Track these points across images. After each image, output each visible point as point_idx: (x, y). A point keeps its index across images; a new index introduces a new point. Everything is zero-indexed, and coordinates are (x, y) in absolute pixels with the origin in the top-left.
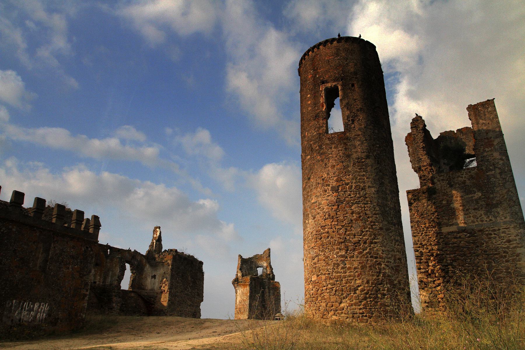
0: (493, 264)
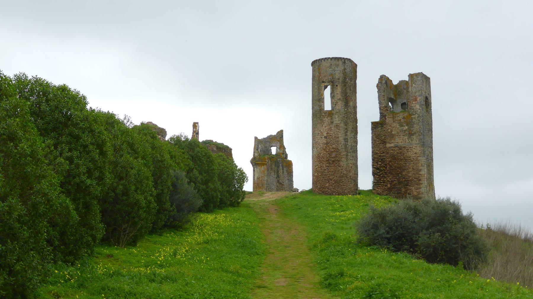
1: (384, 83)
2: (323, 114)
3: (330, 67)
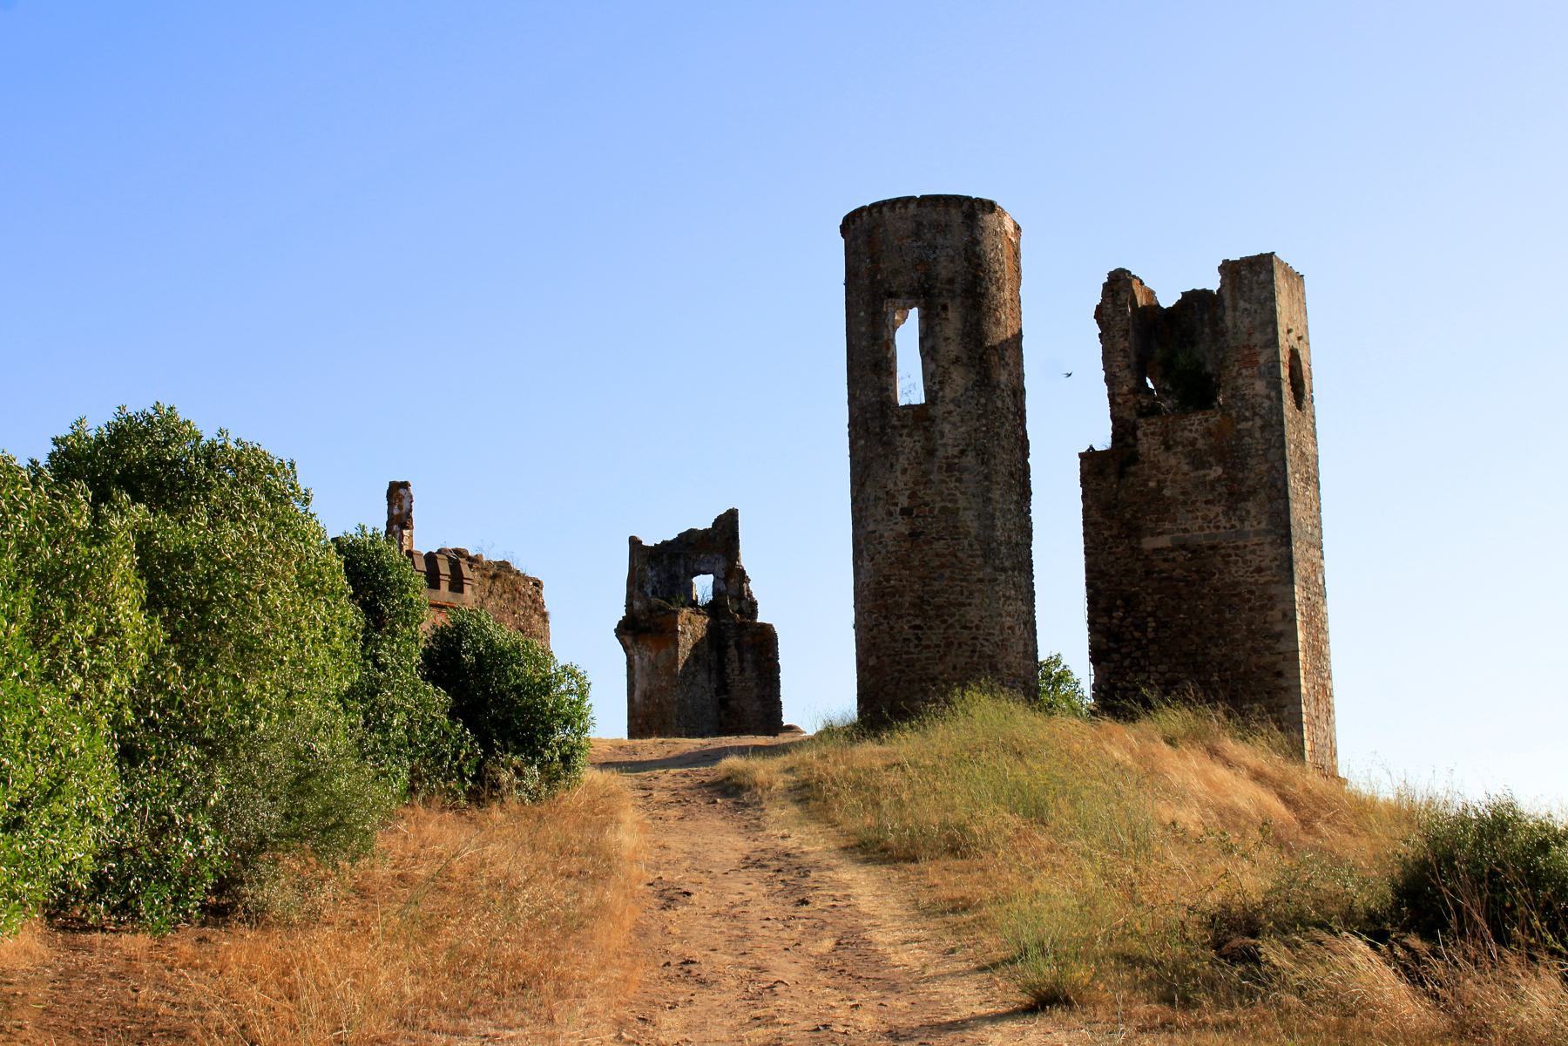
0: (1228, 616)
1: (1123, 310)
2: (895, 421)
3: (917, 235)
